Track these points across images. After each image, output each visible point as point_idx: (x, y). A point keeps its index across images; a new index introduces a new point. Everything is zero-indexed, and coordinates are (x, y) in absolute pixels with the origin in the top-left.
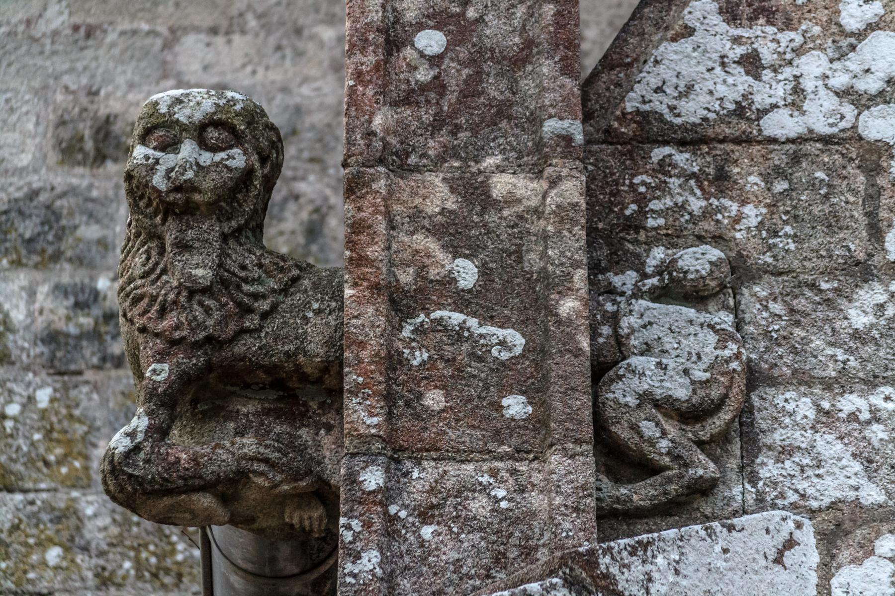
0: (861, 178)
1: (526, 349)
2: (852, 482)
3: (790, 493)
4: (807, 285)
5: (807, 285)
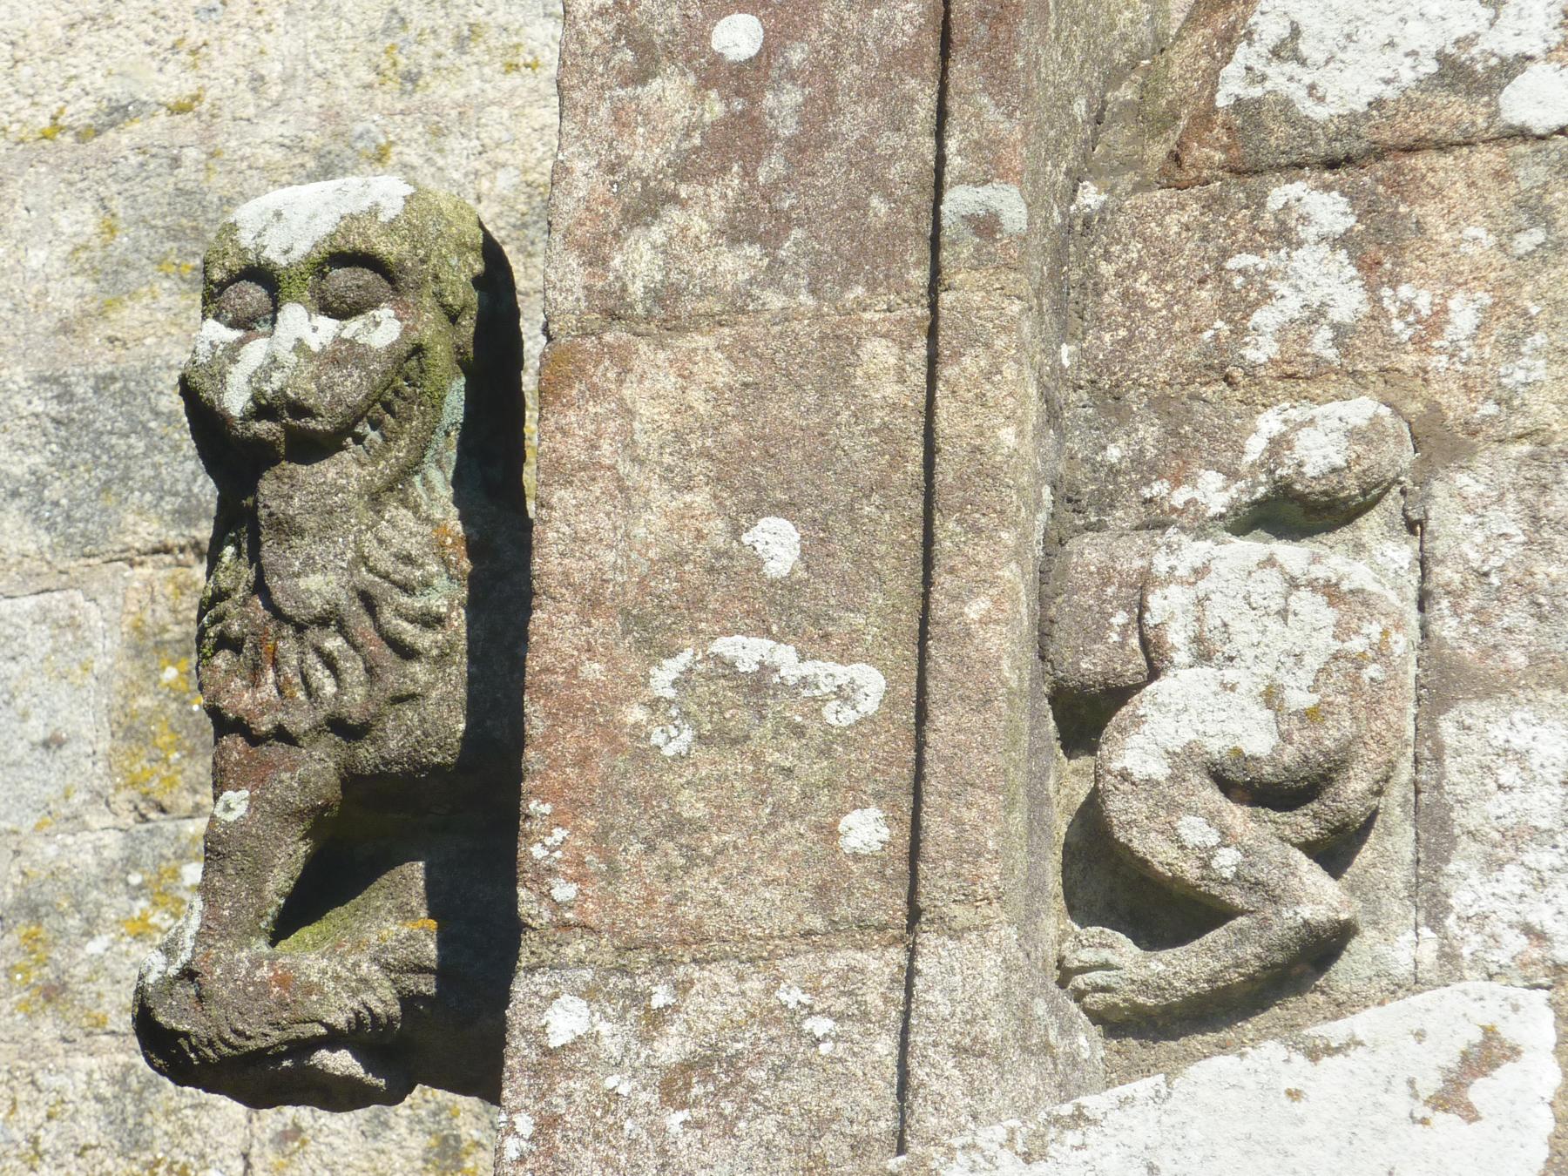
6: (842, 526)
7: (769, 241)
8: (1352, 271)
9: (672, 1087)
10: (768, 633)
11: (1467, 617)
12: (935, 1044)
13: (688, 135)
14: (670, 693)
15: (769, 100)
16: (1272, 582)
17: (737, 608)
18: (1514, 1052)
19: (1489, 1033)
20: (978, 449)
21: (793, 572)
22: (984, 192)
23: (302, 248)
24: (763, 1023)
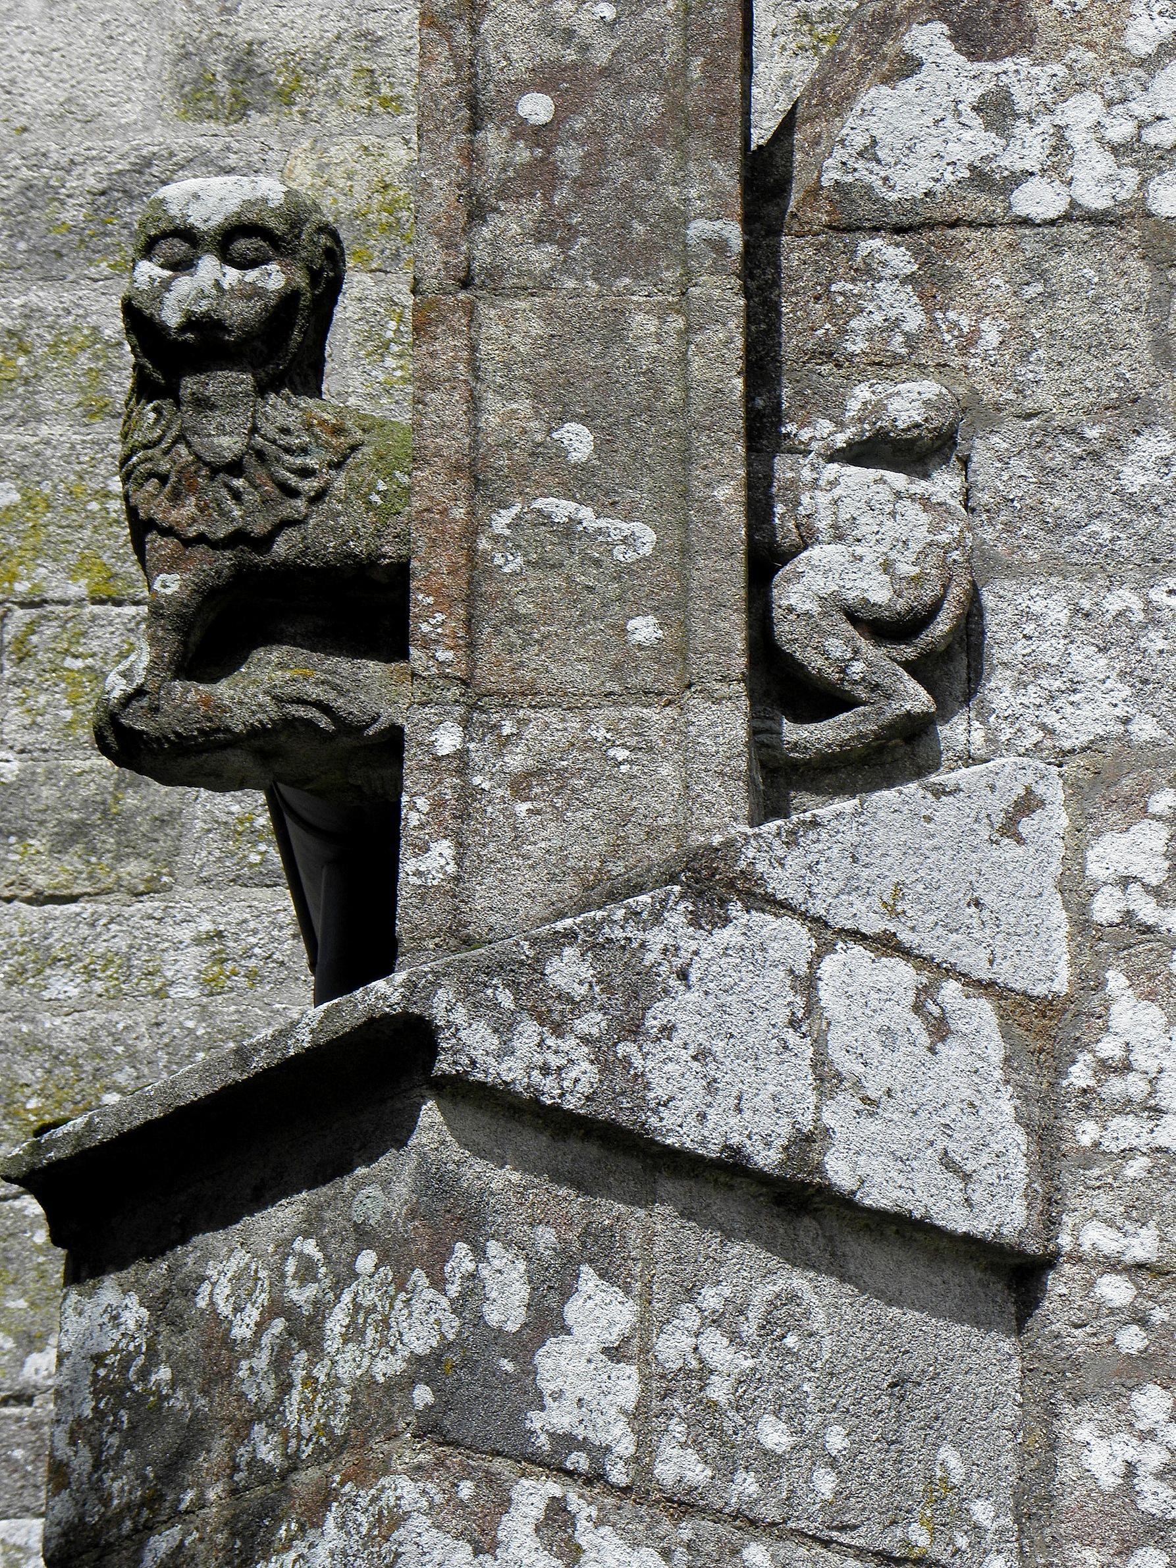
0: (1145, 273)
1: (659, 548)
2: (1120, 712)
3: (1032, 731)
4: (1064, 431)
5: (1064, 431)
6: (621, 432)
7: (564, 244)
8: (915, 300)
9: (520, 785)
10: (573, 498)
11: (1000, 527)
12: (706, 770)
13: (504, 170)
14: (507, 532)
15: (560, 151)
16: (885, 495)
17: (552, 481)
18: (1042, 804)
19: (1029, 791)
20: (720, 391)
21: (589, 460)
22: (718, 225)
23: (217, 220)
24: (581, 750)
